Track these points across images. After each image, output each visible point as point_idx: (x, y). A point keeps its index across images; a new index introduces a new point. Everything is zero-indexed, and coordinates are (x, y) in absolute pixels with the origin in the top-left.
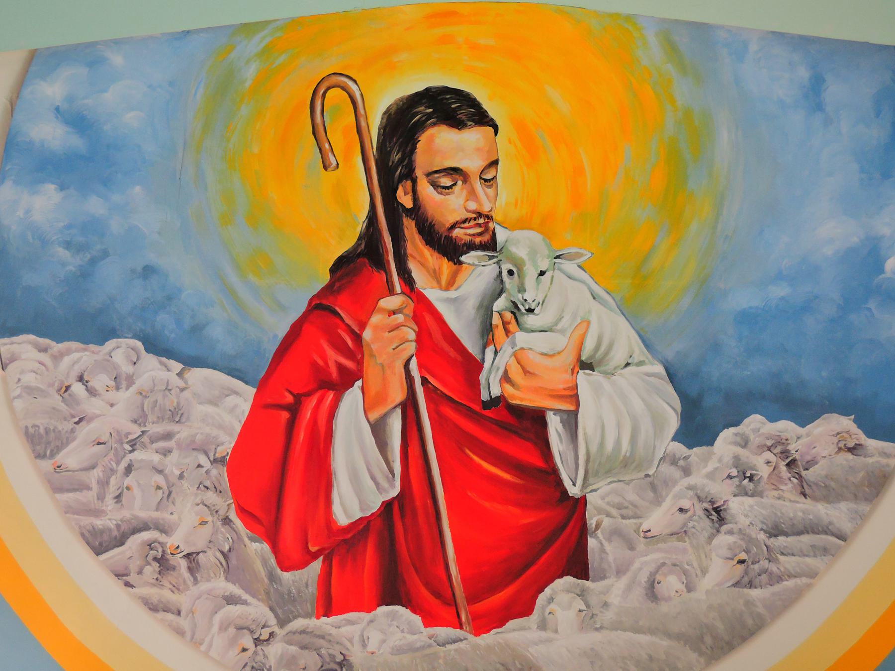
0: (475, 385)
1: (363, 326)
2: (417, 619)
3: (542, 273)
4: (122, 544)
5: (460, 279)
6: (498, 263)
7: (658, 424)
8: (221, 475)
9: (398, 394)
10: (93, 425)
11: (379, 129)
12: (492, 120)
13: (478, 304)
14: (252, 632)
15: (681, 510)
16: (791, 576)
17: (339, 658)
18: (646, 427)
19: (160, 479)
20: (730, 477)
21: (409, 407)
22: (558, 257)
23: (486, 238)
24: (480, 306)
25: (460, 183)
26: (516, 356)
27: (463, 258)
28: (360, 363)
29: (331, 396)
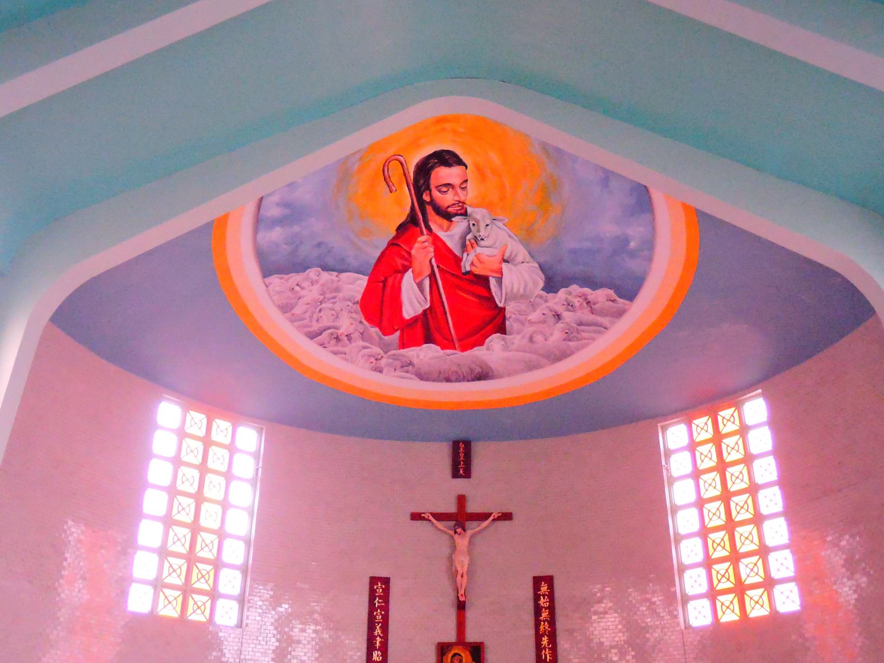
0: (459, 267)
1: (411, 248)
2: (438, 348)
3: (487, 225)
4: (321, 335)
5: (452, 228)
6: (468, 221)
7: (535, 283)
8: (358, 308)
9: (427, 271)
10: (304, 299)
11: (414, 172)
12: (464, 163)
13: (457, 508)
14: (374, 357)
15: (543, 314)
16: (585, 339)
17: (409, 362)
18: (530, 285)
19: (334, 312)
20: (563, 305)
21: (432, 276)
22: (494, 220)
23: (463, 211)
24: (461, 238)
25: (451, 189)
26: (477, 256)
27: (453, 219)
28: (411, 262)
29: (399, 275)
